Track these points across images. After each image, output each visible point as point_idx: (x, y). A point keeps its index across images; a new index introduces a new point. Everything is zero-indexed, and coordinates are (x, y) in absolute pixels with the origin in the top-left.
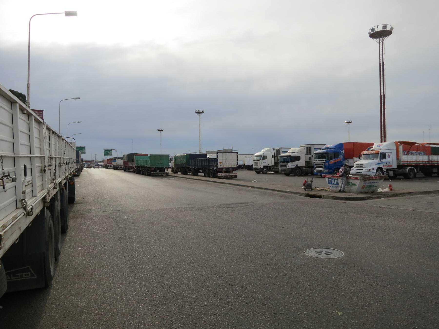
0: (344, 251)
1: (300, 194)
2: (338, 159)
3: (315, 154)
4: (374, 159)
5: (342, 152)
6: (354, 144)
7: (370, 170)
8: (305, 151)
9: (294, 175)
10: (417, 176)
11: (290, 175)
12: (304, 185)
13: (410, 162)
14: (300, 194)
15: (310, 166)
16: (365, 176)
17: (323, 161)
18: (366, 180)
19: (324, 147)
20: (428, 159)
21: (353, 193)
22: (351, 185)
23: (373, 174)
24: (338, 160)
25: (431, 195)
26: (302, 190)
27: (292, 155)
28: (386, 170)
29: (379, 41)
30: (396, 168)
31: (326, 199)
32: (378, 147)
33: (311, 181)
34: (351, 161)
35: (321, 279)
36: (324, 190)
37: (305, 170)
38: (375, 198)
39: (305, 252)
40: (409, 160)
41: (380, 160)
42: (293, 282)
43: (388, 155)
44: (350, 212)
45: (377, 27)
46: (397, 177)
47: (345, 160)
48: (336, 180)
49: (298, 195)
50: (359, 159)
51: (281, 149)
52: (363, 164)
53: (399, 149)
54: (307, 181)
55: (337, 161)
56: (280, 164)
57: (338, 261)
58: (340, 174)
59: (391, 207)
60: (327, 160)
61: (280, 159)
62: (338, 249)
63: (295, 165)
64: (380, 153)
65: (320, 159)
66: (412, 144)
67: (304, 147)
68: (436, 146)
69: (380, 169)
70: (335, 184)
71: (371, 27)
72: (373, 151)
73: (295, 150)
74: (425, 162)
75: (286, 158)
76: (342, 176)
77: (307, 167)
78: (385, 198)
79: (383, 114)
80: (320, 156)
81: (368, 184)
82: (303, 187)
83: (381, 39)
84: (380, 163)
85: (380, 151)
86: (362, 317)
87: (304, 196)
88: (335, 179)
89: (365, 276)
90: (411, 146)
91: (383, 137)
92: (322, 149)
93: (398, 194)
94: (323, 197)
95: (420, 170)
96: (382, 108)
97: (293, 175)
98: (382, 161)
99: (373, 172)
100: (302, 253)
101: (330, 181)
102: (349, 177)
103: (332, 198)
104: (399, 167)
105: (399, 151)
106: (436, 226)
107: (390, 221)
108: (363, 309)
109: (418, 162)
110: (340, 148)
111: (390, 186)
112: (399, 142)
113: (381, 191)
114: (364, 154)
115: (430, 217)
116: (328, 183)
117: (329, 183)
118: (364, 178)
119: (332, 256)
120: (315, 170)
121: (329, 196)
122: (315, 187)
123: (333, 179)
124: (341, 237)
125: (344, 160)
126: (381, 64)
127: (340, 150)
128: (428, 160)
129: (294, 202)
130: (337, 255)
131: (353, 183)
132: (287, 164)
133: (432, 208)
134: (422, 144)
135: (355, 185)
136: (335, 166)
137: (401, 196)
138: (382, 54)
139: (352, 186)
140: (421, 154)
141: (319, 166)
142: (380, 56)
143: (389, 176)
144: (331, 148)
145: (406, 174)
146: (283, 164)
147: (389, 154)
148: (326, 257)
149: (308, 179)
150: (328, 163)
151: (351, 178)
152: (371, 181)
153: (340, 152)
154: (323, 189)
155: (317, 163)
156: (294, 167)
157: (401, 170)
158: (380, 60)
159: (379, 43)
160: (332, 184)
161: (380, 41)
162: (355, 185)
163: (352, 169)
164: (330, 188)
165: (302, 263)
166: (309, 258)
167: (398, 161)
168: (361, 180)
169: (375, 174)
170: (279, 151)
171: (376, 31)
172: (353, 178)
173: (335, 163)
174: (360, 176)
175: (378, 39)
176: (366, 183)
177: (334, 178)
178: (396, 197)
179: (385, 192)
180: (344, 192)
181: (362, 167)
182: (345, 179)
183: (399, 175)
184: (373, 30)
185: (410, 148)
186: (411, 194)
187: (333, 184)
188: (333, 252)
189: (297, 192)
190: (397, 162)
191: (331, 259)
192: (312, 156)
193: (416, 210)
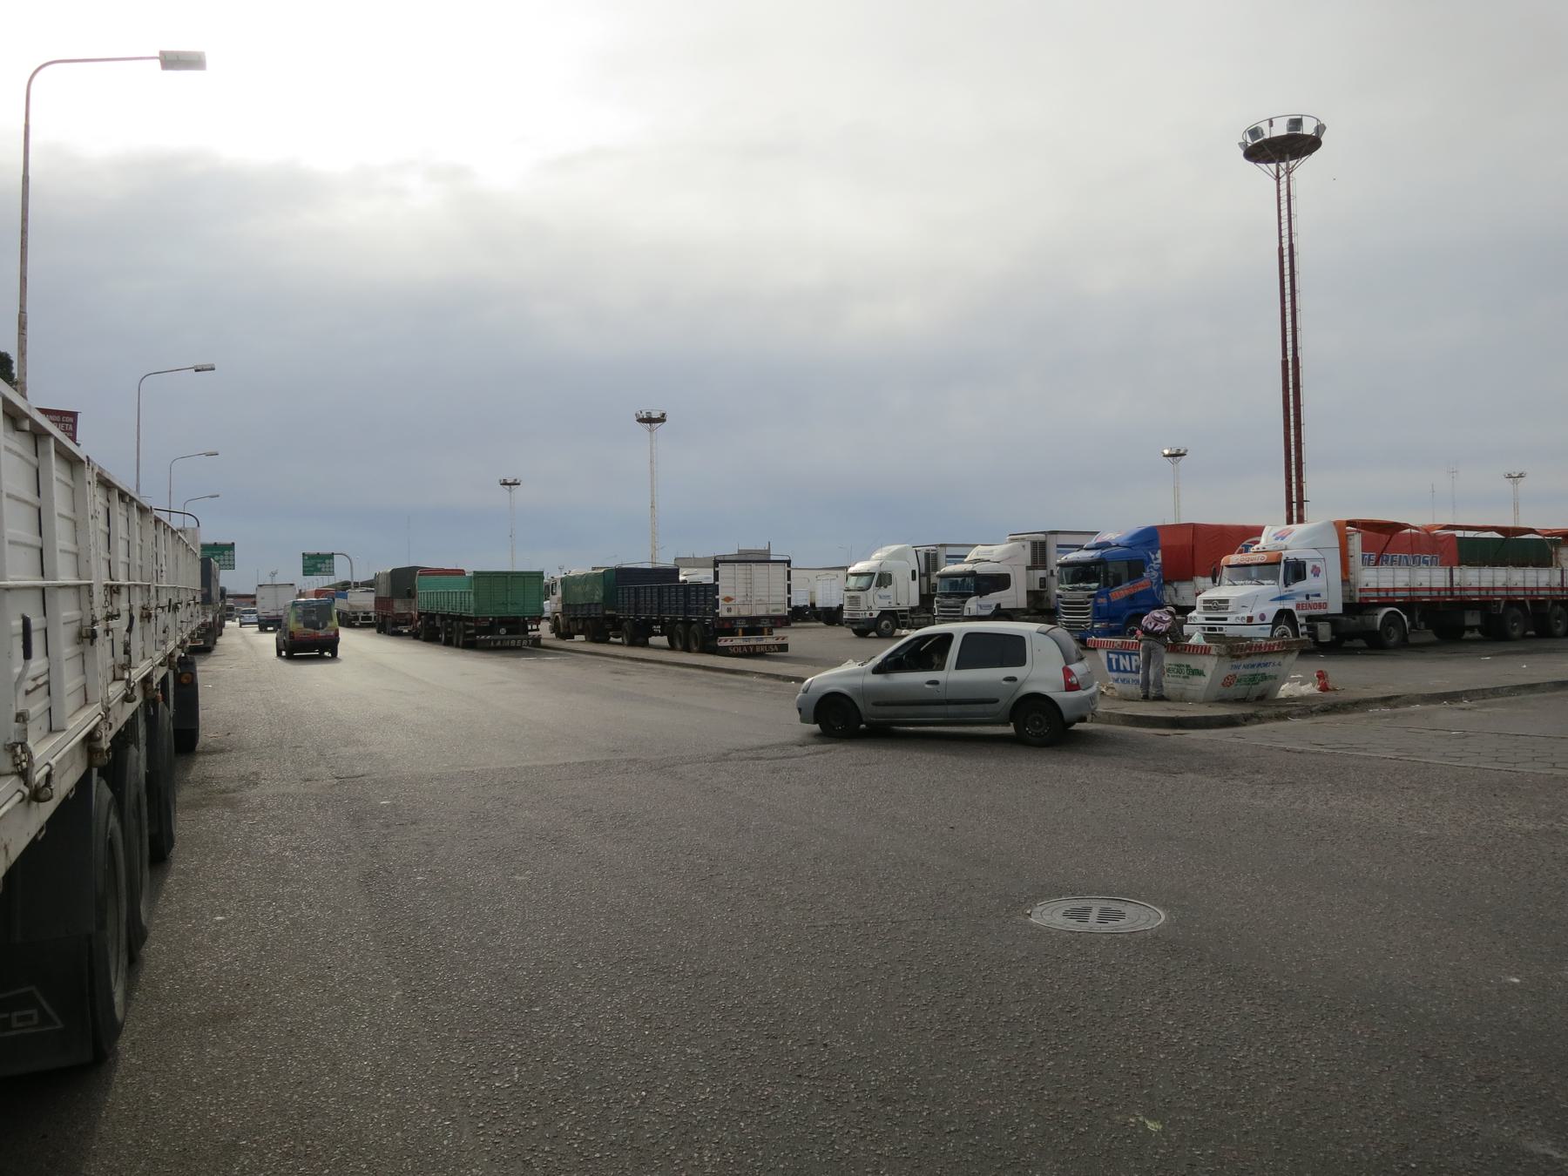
0: (1164, 906)
2: (1142, 583)
3: (1062, 565)
4: (1263, 582)
5: (1156, 559)
6: (1195, 528)
7: (1250, 619)
8: (1026, 556)
10: (1412, 639)
13: (1387, 590)
15: (1045, 607)
18: (1238, 657)
19: (1093, 541)
20: (1448, 579)
21: (1193, 700)
23: (1261, 633)
25: (1462, 705)
27: (981, 568)
28: (1307, 621)
32: (1277, 539)
38: (1270, 718)
39: (1029, 915)
40: (1382, 585)
45: (1271, 124)
46: (1344, 645)
47: (1167, 587)
48: (1134, 658)
50: (1214, 581)
52: (1226, 601)
53: (1351, 547)
56: (938, 602)
65: (1077, 585)
66: (1392, 529)
67: (1023, 543)
69: (1284, 616)
70: (1131, 672)
71: (1249, 124)
72: (1261, 555)
73: (992, 551)
74: (1439, 590)
77: (1033, 611)
80: (1080, 573)
81: (1243, 669)
83: (1283, 165)
85: (1285, 554)
88: (1130, 655)
91: (1295, 505)
92: (1087, 549)
93: (1349, 704)
96: (1291, 405)
99: (1261, 629)
100: (1018, 918)
101: (1114, 661)
104: (1351, 608)
105: (1351, 553)
106: (1478, 813)
111: (1321, 675)
112: (1351, 523)
114: (1229, 566)
116: (1107, 669)
117: (1111, 669)
118: (1232, 650)
119: (1123, 925)
123: (1124, 654)
125: (1161, 588)
126: (1286, 252)
127: (1149, 549)
128: (1448, 585)
132: (964, 602)
134: (1426, 530)
135: (1200, 673)
136: (1130, 608)
139: (1191, 677)
140: (1426, 562)
142: (1280, 224)
144: (1118, 545)
146: (951, 601)
147: (1315, 563)
148: (1104, 928)
150: (1108, 598)
151: (1185, 650)
152: (1256, 660)
157: (1358, 618)
159: (1278, 178)
161: (1282, 173)
162: (1200, 673)
164: (1115, 685)
165: (1021, 951)
166: (1044, 933)
167: (1347, 588)
168: (1220, 655)
169: (1268, 634)
170: (935, 556)
171: (1267, 136)
173: (1131, 597)
175: (1273, 166)
179: (1302, 698)
183: (1352, 636)
184: (1254, 132)
187: (1125, 671)
188: (1129, 910)
190: (1343, 591)
191: (1120, 936)
192: (1052, 572)
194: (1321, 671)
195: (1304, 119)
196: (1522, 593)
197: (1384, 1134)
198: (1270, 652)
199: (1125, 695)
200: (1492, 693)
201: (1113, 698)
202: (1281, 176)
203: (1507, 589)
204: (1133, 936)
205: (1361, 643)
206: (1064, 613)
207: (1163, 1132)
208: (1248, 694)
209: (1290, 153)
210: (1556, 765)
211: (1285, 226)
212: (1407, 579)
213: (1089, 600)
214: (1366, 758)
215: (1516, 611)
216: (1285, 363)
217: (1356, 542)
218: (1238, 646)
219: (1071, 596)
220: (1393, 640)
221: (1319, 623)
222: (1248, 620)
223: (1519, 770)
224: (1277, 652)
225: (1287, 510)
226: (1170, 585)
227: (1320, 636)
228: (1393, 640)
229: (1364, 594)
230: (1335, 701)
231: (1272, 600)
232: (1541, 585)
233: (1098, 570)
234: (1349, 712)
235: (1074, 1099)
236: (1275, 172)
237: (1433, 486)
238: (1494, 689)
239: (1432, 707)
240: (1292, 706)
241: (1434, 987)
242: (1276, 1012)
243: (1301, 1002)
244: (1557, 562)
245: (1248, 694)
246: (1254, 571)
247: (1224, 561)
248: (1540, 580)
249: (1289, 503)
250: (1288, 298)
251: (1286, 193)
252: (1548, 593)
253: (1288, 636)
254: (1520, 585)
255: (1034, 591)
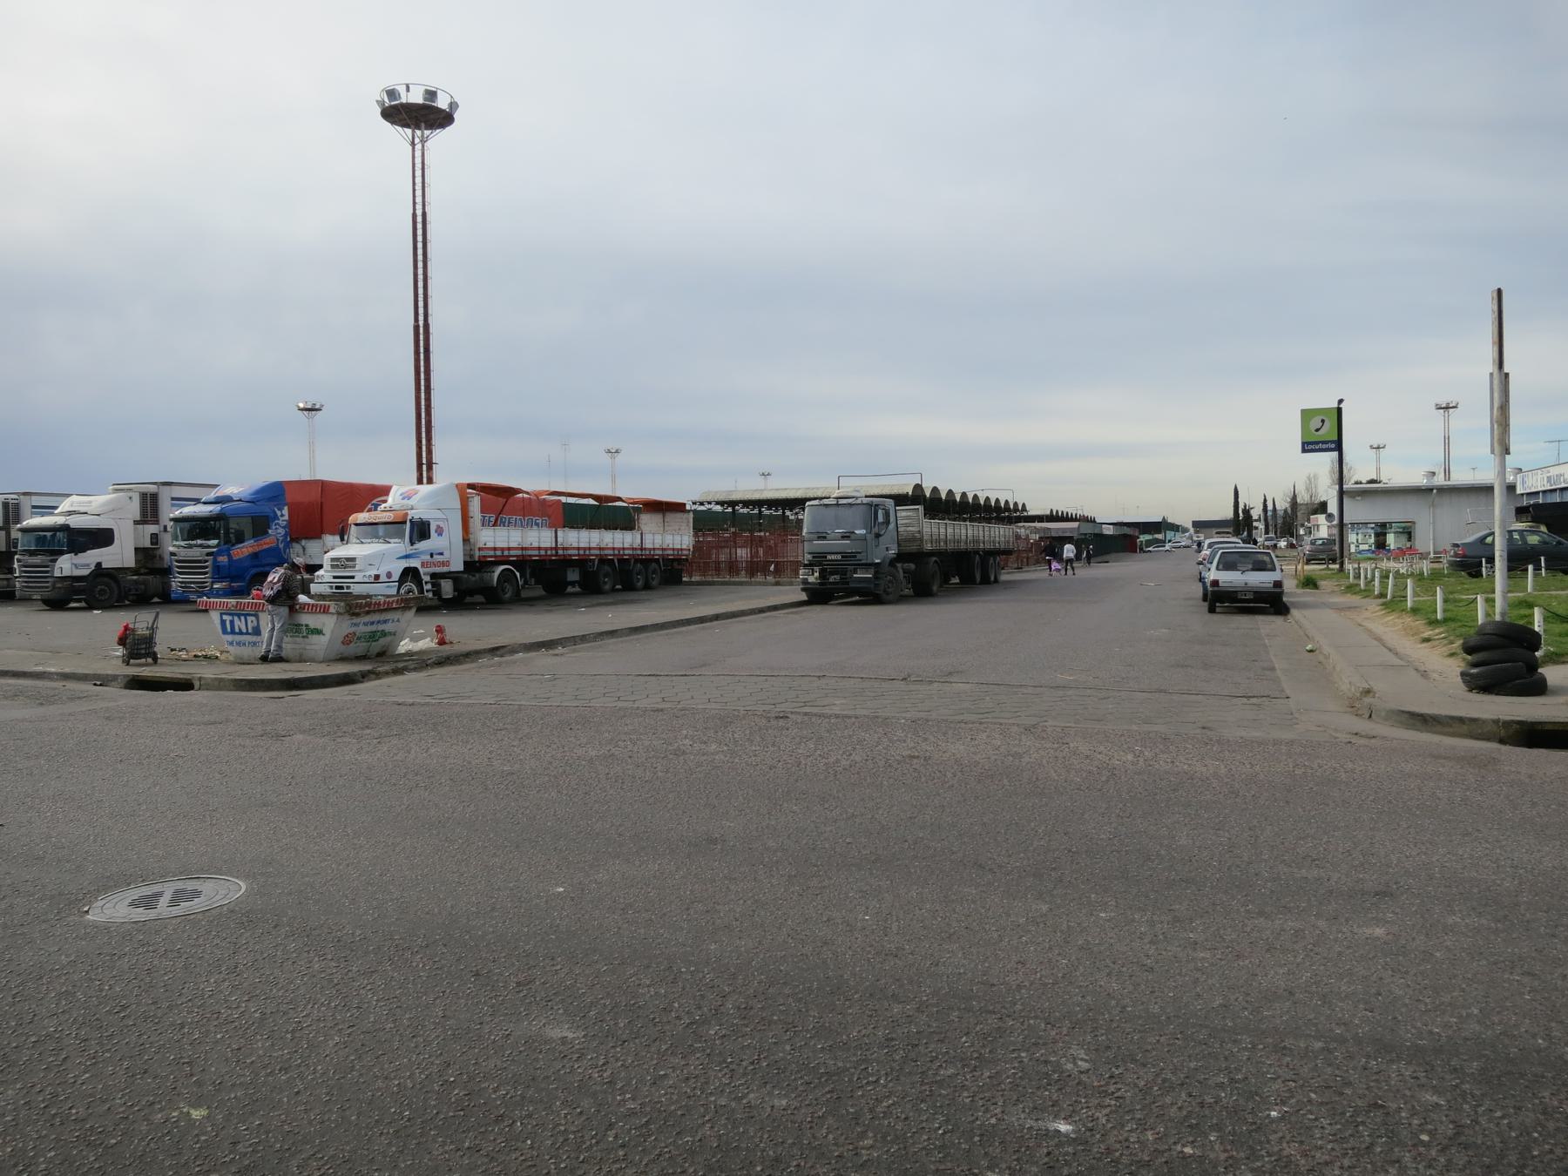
0: (246, 877)
1: (104, 681)
2: (267, 540)
3: (176, 520)
4: (390, 540)
5: (282, 515)
6: (324, 485)
7: (377, 577)
8: (134, 509)
9: (958, 581)
10: (524, 594)
11: (67, 604)
12: (120, 645)
13: (503, 549)
14: (104, 681)
15: (157, 566)
16: (355, 599)
17: (209, 547)
18: (357, 615)
19: (212, 495)
20: (554, 539)
21: (313, 660)
22: (305, 634)
23: (388, 590)
24: (267, 542)
25: (556, 651)
26: (114, 662)
27: (75, 522)
28: (431, 579)
29: (413, 138)
30: (462, 569)
31: (206, 693)
32: (403, 499)
33: (150, 626)
34: (313, 547)
35: (138, 1004)
36: (205, 657)
37: (136, 582)
38: (387, 674)
39: (87, 912)
40: (499, 545)
41: (412, 543)
42: (14, 1045)
43: (435, 527)
44: (292, 732)
45: (408, 89)
46: (466, 601)
47: (294, 545)
48: (250, 619)
49: (95, 685)
50: (342, 539)
51: (28, 497)
52: (353, 559)
53: (471, 508)
54: (131, 626)
55: (261, 548)
56: (19, 561)
57: (218, 918)
58: (268, 593)
59: (434, 701)
60: (222, 543)
61: (22, 539)
62: (227, 876)
63: (88, 565)
64: (410, 520)
65: (194, 542)
66: (508, 492)
67: (130, 494)
68: (577, 502)
69: (410, 574)
70: (247, 633)
71: (389, 83)
72: (388, 514)
73: (90, 502)
74: (546, 549)
75: (49, 538)
76: (272, 600)
77: (143, 571)
78: (420, 671)
79: (423, 388)
80: (197, 528)
81: (363, 626)
82: (117, 650)
83: (418, 132)
84: (412, 554)
85: (411, 514)
86: (280, 1100)
87: (122, 685)
88: (245, 615)
89: (308, 952)
90: (505, 500)
91: (424, 467)
92: (205, 503)
93: (463, 655)
94: (197, 684)
95: (532, 575)
96: (422, 369)
97: (83, 604)
98: (416, 546)
99: (388, 587)
100: (72, 918)
101: (228, 623)
102: (298, 607)
103: (234, 686)
104: (470, 565)
105: (471, 514)
106: (555, 746)
107: (423, 747)
108: (286, 1070)
109: (526, 549)
110: (270, 499)
111: (440, 630)
112: (471, 486)
113: (410, 647)
114: (356, 525)
115: (542, 719)
116: (220, 631)
117: (224, 631)
118: (351, 608)
119: (197, 905)
120: (176, 582)
121: (221, 679)
122: (172, 650)
123: (239, 616)
124: (243, 828)
125: (288, 545)
126: (419, 219)
127: (275, 506)
128: (554, 546)
129: (70, 714)
130: (218, 897)
131: (312, 626)
132: (55, 561)
133: (550, 691)
134: (536, 495)
135: (319, 632)
136: (254, 567)
137: (467, 662)
138: (421, 185)
139: (310, 636)
140: (537, 525)
141: (190, 566)
142: (414, 190)
143: (440, 598)
144: (240, 500)
145: (492, 587)
146: (37, 560)
147: (438, 523)
148: (175, 911)
149: (140, 620)
150: (229, 556)
151: (304, 609)
152: (376, 617)
153: (272, 515)
154: (204, 653)
155: (182, 553)
156: (85, 572)
157: (477, 575)
158: (414, 203)
159: (413, 144)
160: (238, 634)
161: (417, 140)
162: (319, 632)
163: (318, 576)
164: (230, 648)
165: (67, 956)
166: (105, 928)
167: (468, 548)
168: (339, 613)
169: (394, 591)
170: (17, 507)
171: (404, 100)
172: (313, 609)
173: (255, 555)
174: (335, 600)
175: (409, 131)
176: (356, 625)
177: (243, 610)
178: (455, 665)
179: (421, 652)
180: (279, 659)
181: (350, 567)
182: (284, 611)
183: (472, 593)
184: (392, 93)
185: (504, 505)
186: (498, 653)
187: (241, 633)
188: (207, 887)
189: (91, 672)
190: (464, 550)
191: (192, 917)
192: (165, 527)
193: (504, 702)
194: (439, 626)
195: (439, 92)
196: (611, 552)
197: (430, 1057)
198: (389, 609)
199: (241, 659)
200: (581, 640)
201: (228, 663)
202: (416, 142)
203: (600, 549)
204: (207, 914)
205: (479, 598)
206: (179, 573)
207: (208, 1117)
208: (368, 651)
209: (425, 122)
210: (621, 699)
211: (419, 193)
212: (520, 540)
213: (206, 558)
214: (469, 705)
215: (607, 568)
216: (416, 328)
217: (475, 504)
218: (357, 603)
219: (184, 554)
220: (507, 596)
221: (442, 581)
222: (375, 579)
223: (592, 705)
224: (395, 608)
225: (417, 471)
226: (297, 542)
227: (443, 593)
228: (507, 596)
229: (483, 553)
230: (448, 653)
231: (398, 559)
232: (626, 546)
233: (218, 525)
234: (461, 663)
235: (109, 1109)
236: (411, 138)
237: (549, 456)
238: (583, 636)
239: (533, 654)
240: (409, 660)
241: (493, 909)
242: (346, 963)
243: (371, 948)
244: (639, 527)
245: (368, 651)
246: (381, 529)
247: (352, 519)
248: (625, 541)
249: (420, 465)
250: (420, 265)
251: (420, 161)
252: (631, 552)
253: (414, 594)
254: (610, 545)
255: (144, 548)
